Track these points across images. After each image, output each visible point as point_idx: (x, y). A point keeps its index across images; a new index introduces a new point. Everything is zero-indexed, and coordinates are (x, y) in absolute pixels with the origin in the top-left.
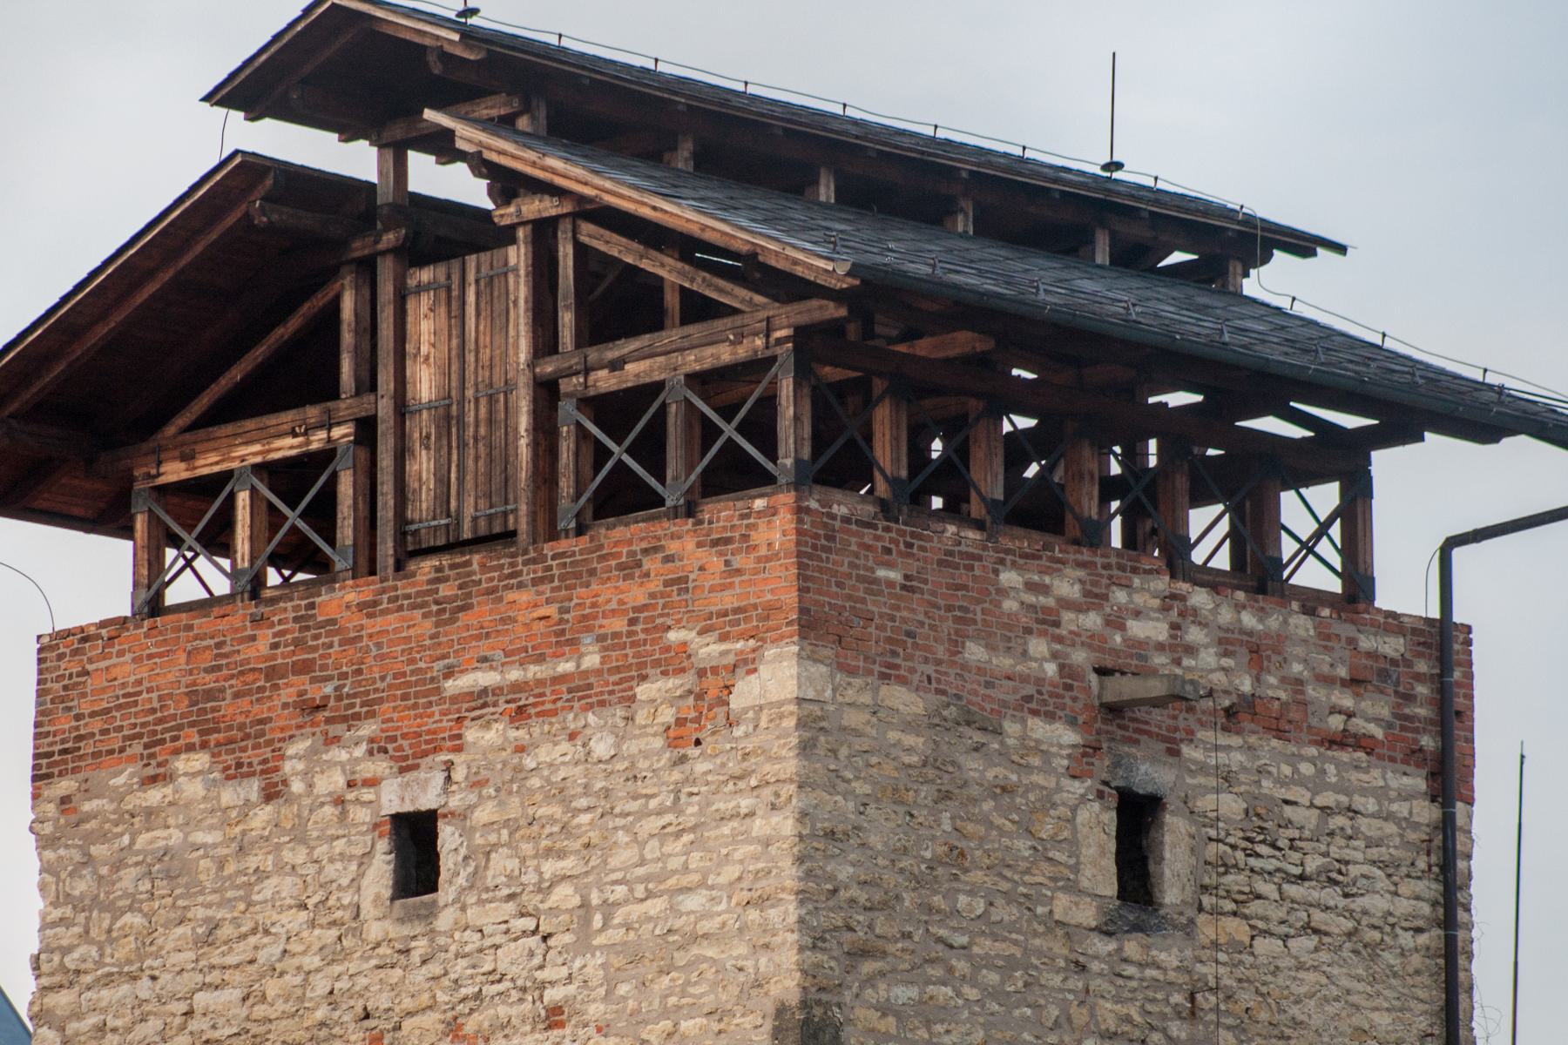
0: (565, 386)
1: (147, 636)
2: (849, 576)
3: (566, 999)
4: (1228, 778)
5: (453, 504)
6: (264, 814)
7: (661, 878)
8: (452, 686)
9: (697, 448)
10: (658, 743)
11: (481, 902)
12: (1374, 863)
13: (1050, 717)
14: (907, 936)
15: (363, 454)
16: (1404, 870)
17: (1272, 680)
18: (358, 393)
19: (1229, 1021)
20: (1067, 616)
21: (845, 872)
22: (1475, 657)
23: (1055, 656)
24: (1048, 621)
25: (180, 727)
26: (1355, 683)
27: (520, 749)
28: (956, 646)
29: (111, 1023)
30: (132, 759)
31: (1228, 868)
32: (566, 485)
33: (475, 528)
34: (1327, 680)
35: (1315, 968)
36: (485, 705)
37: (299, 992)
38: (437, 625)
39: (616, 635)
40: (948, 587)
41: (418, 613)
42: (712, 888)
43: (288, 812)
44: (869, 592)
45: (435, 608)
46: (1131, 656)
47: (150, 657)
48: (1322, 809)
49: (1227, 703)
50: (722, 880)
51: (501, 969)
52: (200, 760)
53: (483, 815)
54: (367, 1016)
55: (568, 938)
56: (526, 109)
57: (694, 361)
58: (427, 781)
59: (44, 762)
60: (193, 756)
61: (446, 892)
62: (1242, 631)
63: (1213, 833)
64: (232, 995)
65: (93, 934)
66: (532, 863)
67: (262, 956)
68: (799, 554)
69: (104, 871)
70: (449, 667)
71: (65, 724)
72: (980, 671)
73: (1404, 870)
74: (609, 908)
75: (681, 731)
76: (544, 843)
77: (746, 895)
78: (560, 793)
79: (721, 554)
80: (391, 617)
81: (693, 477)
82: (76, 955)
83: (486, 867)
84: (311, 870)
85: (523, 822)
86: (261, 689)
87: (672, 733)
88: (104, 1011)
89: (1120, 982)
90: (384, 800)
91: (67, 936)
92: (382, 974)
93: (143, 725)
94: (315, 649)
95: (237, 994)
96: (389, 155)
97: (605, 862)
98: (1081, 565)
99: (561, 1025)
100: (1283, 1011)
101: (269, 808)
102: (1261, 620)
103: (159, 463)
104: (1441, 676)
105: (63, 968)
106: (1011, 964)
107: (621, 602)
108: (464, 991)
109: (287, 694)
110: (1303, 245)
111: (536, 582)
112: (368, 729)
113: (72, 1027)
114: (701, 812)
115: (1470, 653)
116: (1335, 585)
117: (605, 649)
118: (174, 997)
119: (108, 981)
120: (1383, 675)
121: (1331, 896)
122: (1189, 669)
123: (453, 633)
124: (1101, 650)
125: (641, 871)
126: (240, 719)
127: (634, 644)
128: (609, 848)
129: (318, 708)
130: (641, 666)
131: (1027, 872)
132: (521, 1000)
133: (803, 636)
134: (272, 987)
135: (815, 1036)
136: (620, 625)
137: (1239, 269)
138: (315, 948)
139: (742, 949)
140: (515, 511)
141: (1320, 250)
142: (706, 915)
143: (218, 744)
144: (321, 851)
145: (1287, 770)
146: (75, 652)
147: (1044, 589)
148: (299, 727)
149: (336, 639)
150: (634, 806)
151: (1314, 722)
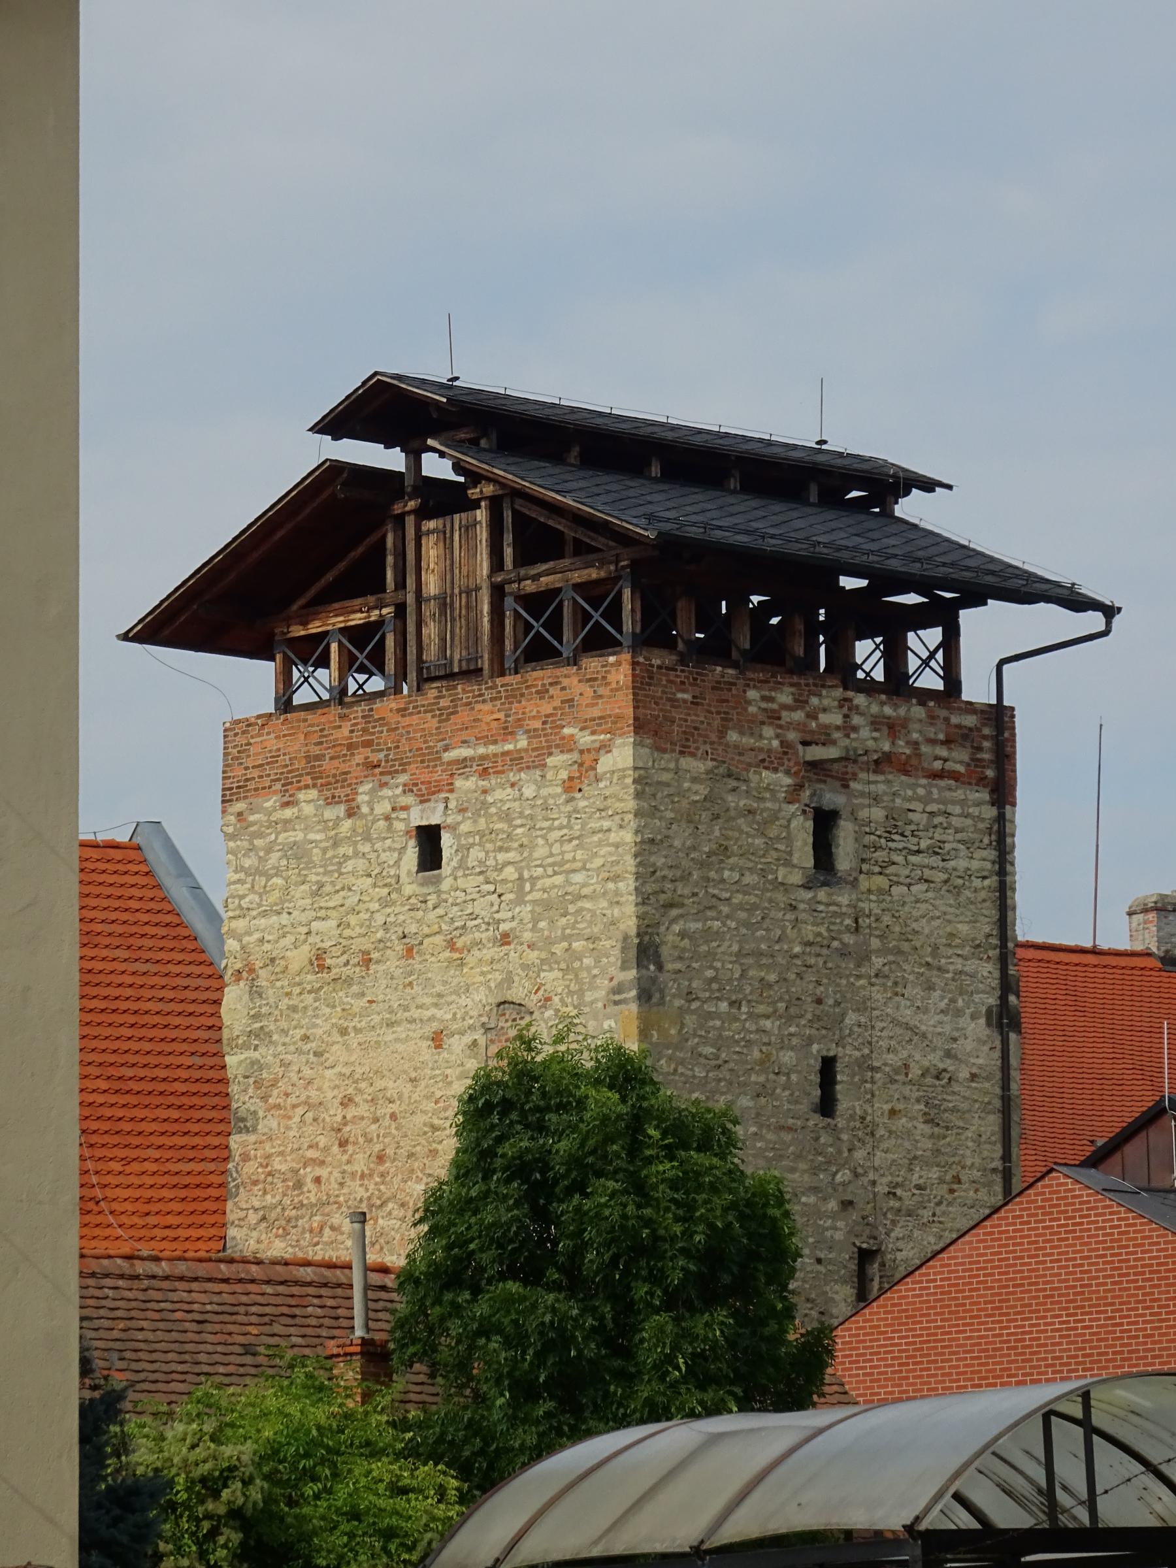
0: (507, 588)
1: (283, 724)
2: (661, 698)
3: (511, 929)
4: (876, 799)
5: (448, 652)
6: (347, 824)
7: (561, 864)
8: (448, 756)
9: (580, 626)
10: (559, 790)
11: (465, 876)
12: (959, 841)
13: (776, 770)
14: (695, 895)
15: (399, 623)
16: (977, 844)
17: (901, 743)
18: (396, 589)
19: (877, 933)
20: (784, 714)
21: (661, 862)
22: (1017, 725)
23: (777, 736)
24: (773, 717)
25: (301, 775)
26: (947, 742)
27: (485, 792)
28: (722, 733)
29: (267, 937)
30: (275, 792)
31: (877, 848)
32: (508, 645)
33: (460, 666)
34: (932, 742)
35: (926, 901)
36: (466, 767)
37: (367, 923)
38: (439, 722)
39: (535, 730)
40: (718, 701)
41: (429, 715)
42: (588, 870)
43: (360, 823)
44: (672, 706)
45: (438, 712)
46: (821, 734)
47: (284, 736)
48: (930, 813)
49: (875, 757)
50: (593, 866)
51: (476, 912)
52: (313, 794)
53: (465, 828)
54: (405, 937)
55: (512, 896)
56: (485, 434)
57: (577, 577)
58: (435, 808)
59: (228, 793)
60: (309, 791)
61: (446, 869)
62: (884, 717)
63: (867, 830)
64: (333, 923)
65: (256, 888)
66: (492, 854)
67: (348, 903)
68: (634, 688)
69: (262, 854)
70: (446, 745)
71: (239, 772)
72: (736, 747)
73: (977, 844)
74: (533, 880)
75: (571, 784)
76: (499, 844)
77: (607, 875)
78: (507, 817)
79: (591, 687)
80: (415, 717)
81: (578, 641)
82: (247, 900)
83: (468, 856)
84: (373, 856)
85: (487, 832)
86: (345, 755)
87: (567, 785)
88: (263, 931)
89: (815, 914)
90: (412, 818)
91: (241, 889)
92: (412, 914)
93: (282, 773)
94: (373, 734)
95: (334, 923)
96: (412, 457)
97: (531, 854)
98: (792, 685)
99: (508, 943)
100: (906, 926)
101: (350, 821)
102: (895, 710)
103: (288, 627)
104: (997, 736)
105: (240, 907)
106: (754, 907)
107: (538, 712)
108: (457, 924)
109: (358, 759)
110: (928, 485)
111: (492, 699)
112: (403, 778)
113: (246, 939)
114: (583, 828)
115: (1014, 722)
116: (939, 685)
117: (529, 737)
118: (300, 924)
119: (264, 914)
120: (965, 737)
121: (935, 861)
122: (854, 739)
123: (448, 727)
124: (804, 731)
125: (550, 860)
126: (334, 771)
127: (545, 735)
128: (533, 847)
129: (375, 766)
130: (549, 747)
131: (764, 856)
132: (487, 930)
133: (636, 733)
134: (353, 920)
135: (645, 951)
136: (537, 724)
137: (893, 499)
138: (376, 899)
139: (605, 904)
140: (482, 657)
141: (937, 489)
142: (584, 885)
143: (322, 785)
144: (378, 846)
145: (910, 793)
146: (244, 732)
147: (771, 699)
148: (366, 777)
149: (385, 729)
150: (546, 824)
151: (925, 765)
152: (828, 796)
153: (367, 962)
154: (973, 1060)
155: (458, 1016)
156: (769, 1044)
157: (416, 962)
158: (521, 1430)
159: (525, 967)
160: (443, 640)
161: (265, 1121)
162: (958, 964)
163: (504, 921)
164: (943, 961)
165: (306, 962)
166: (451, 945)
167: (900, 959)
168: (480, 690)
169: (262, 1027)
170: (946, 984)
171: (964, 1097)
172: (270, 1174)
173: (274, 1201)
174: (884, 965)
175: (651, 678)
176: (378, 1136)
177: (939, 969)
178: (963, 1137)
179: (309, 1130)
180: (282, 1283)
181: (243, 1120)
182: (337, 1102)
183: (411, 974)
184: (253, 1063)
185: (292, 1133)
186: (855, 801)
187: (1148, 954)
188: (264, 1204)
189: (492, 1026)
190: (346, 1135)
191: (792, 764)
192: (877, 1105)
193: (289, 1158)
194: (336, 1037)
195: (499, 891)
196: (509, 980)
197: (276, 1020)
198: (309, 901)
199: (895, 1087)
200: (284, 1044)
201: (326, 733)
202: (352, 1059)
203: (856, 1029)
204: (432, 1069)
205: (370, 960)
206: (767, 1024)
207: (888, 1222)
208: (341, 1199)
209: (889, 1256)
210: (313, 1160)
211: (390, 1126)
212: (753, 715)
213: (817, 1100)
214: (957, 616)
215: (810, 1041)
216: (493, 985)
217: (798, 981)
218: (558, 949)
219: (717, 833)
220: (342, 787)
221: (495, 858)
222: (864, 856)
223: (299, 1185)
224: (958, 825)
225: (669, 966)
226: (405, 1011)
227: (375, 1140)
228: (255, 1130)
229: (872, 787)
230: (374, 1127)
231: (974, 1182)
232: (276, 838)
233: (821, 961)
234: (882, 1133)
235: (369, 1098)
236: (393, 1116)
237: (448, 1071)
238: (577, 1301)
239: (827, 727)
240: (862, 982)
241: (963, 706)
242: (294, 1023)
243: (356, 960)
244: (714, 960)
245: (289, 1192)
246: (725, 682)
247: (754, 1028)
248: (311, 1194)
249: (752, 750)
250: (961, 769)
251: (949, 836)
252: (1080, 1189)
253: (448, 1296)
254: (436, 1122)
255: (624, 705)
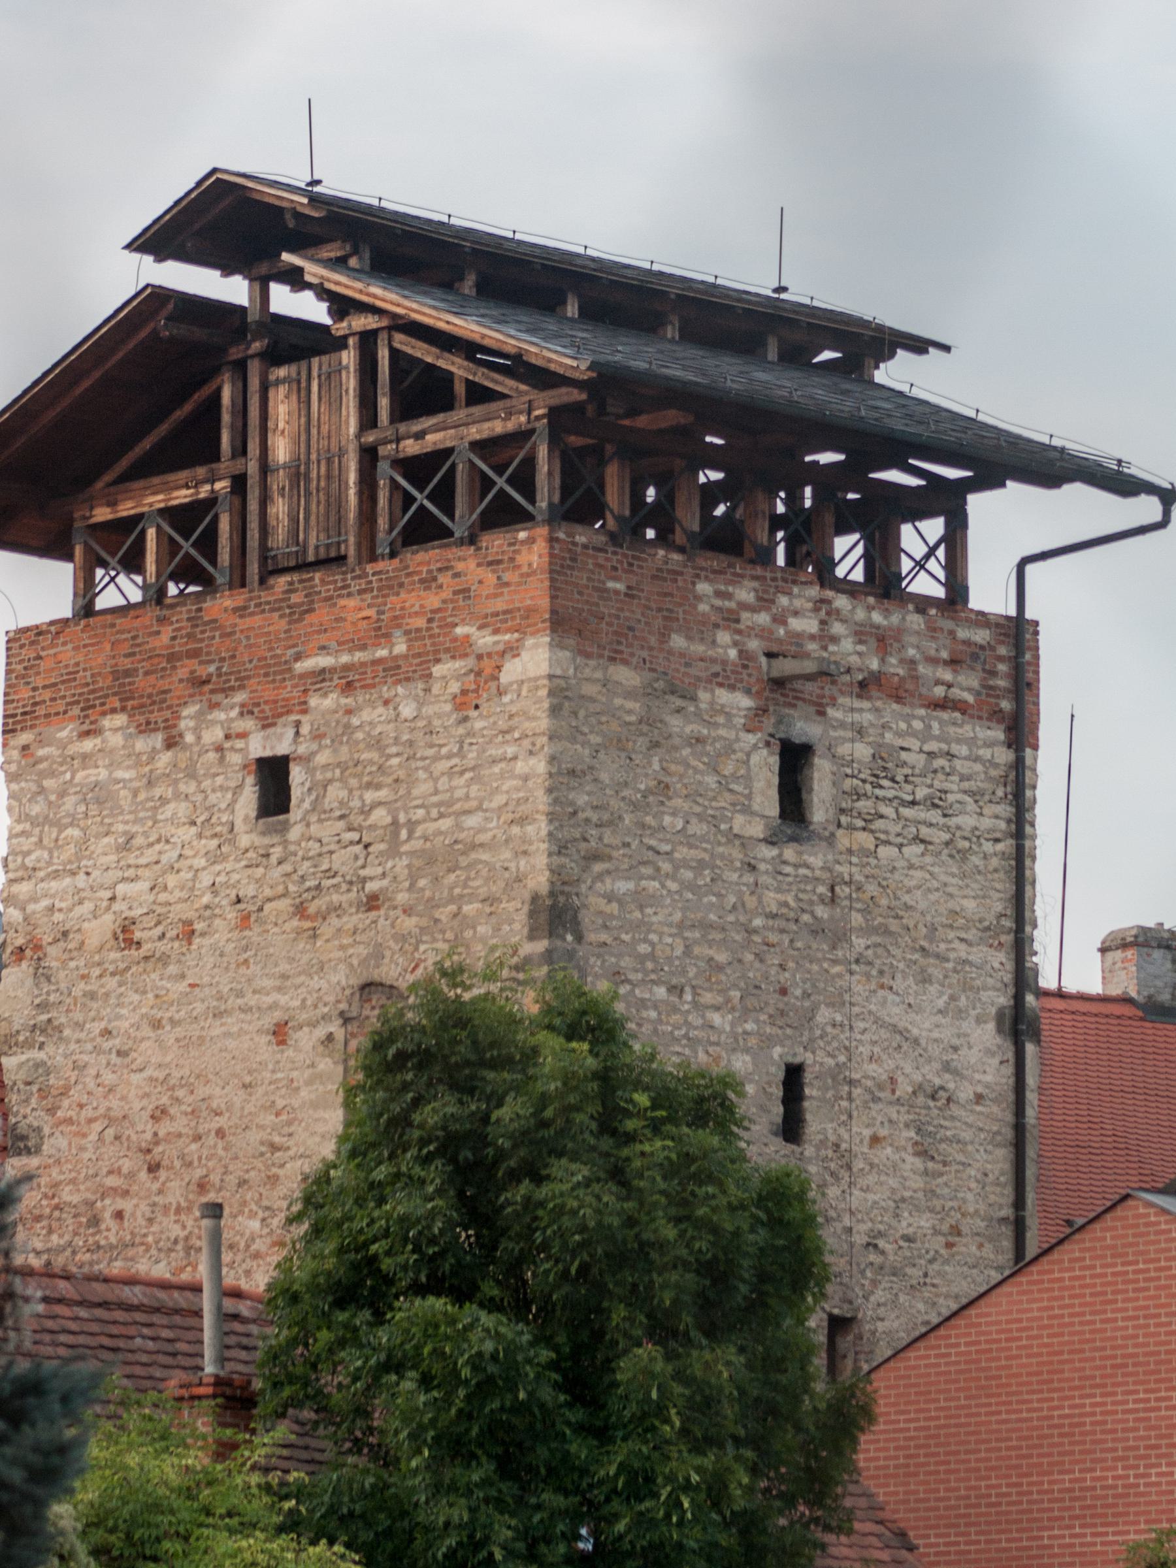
0: (383, 451)
1: (83, 631)
3: (381, 889)
4: (860, 732)
5: (301, 536)
6: (165, 758)
8: (300, 667)
9: (477, 497)
10: (448, 707)
11: (320, 821)
12: (965, 792)
13: (732, 688)
14: (627, 845)
15: (237, 501)
17: (893, 661)
18: (234, 457)
19: (859, 906)
20: (745, 615)
21: (582, 799)
22: (1041, 644)
24: (731, 619)
25: (106, 696)
26: (953, 663)
27: (349, 712)
28: (664, 637)
29: (58, 905)
30: (72, 719)
32: (382, 523)
34: (933, 661)
36: (324, 680)
37: (190, 884)
38: (290, 623)
39: (418, 630)
40: (659, 594)
41: (276, 615)
42: (486, 811)
44: (601, 598)
46: (791, 644)
47: (85, 646)
48: (929, 754)
49: (860, 677)
52: (120, 720)
53: (322, 758)
54: (239, 901)
55: (383, 846)
56: (355, 252)
57: (476, 432)
58: (282, 735)
60: (116, 716)
61: (295, 814)
63: (849, 771)
64: (143, 886)
65: (46, 841)
66: (357, 793)
67: (164, 859)
68: (551, 571)
69: (53, 798)
71: (25, 693)
72: (682, 655)
73: (987, 797)
74: (412, 825)
76: (366, 779)
77: (510, 816)
79: (494, 571)
80: (257, 618)
81: (474, 516)
82: (33, 857)
85: (351, 764)
86: (164, 669)
87: (458, 700)
89: (780, 878)
90: (251, 748)
93: (80, 694)
94: (202, 640)
95: (146, 885)
97: (409, 793)
98: (755, 578)
99: (377, 908)
100: (897, 898)
101: (169, 754)
102: (886, 617)
103: (92, 509)
104: (1016, 657)
105: (24, 866)
106: (701, 865)
107: (422, 606)
108: (308, 884)
109: (183, 673)
110: (919, 345)
112: (240, 697)
113: (31, 908)
114: (478, 757)
116: (940, 592)
117: (410, 640)
119: (55, 875)
121: (934, 816)
124: (769, 639)
125: (435, 799)
126: (149, 690)
127: (431, 637)
128: (412, 782)
130: (436, 652)
131: (714, 799)
132: (349, 890)
133: (553, 630)
134: (172, 880)
136: (421, 622)
137: (872, 363)
139: (507, 854)
140: (346, 541)
141: (931, 349)
143: (133, 708)
144: (206, 784)
145: (903, 726)
146: (32, 643)
147: (728, 596)
148: (191, 696)
150: (431, 752)
151: (924, 691)
152: (799, 725)
153: (189, 934)
154: (977, 1076)
155: (309, 1003)
156: (717, 1044)
157: (253, 934)
158: (444, 1501)
159: (402, 938)
160: (294, 520)
161: (52, 1140)
162: (962, 950)
163: (371, 879)
164: (943, 946)
165: (109, 935)
166: (300, 910)
167: (887, 940)
168: (344, 580)
169: (49, 1020)
170: (946, 977)
171: (966, 1123)
172: (57, 1207)
173: (62, 1242)
174: (868, 947)
175: (574, 560)
176: (200, 1158)
177: (937, 956)
178: (965, 1176)
179: (110, 1151)
180: (99, 1305)
181: (24, 1138)
182: (146, 1115)
183: (246, 949)
184: (37, 1065)
185: (86, 1156)
186: (832, 733)
187: (1126, 1000)
188: (49, 1245)
189: (354, 1014)
190: (158, 1158)
191: (753, 680)
192: (854, 1129)
193: (82, 1187)
194: (147, 1031)
195: (366, 839)
196: (377, 955)
197: (68, 1011)
198: (114, 858)
199: (875, 1107)
200: (78, 1041)
201: (139, 641)
202: (168, 1059)
203: (829, 1029)
204: (273, 1072)
205: (193, 932)
206: (716, 1018)
207: (866, 1283)
208: (150, 1239)
209: (867, 1327)
210: (114, 1190)
211: (215, 1146)
212: (703, 614)
213: (779, 1120)
214: (965, 503)
215: (768, 1041)
216: (355, 962)
217: (757, 965)
218: (444, 914)
219: (656, 766)
220: (161, 710)
221: (361, 798)
222: (844, 805)
223: (95, 1221)
224: (965, 771)
225: (592, 937)
226: (237, 996)
227: (196, 1163)
228: (38, 1150)
229: (857, 717)
230: (194, 1147)
231: (978, 1234)
232: (73, 777)
233: (786, 939)
234: (861, 1166)
235: (189, 1109)
236: (220, 1133)
237: (295, 1074)
238: (528, 1323)
239: (799, 635)
240: (837, 969)
241: (973, 616)
242: (92, 1014)
243: (174, 932)
244: (649, 931)
245: (82, 1230)
246: (669, 571)
247: (700, 1022)
248: (111, 1232)
249: (702, 660)
250: (970, 699)
251: (953, 784)
252: (1166, 1222)
253: (342, 1317)
254: (277, 1139)
255: (537, 595)
